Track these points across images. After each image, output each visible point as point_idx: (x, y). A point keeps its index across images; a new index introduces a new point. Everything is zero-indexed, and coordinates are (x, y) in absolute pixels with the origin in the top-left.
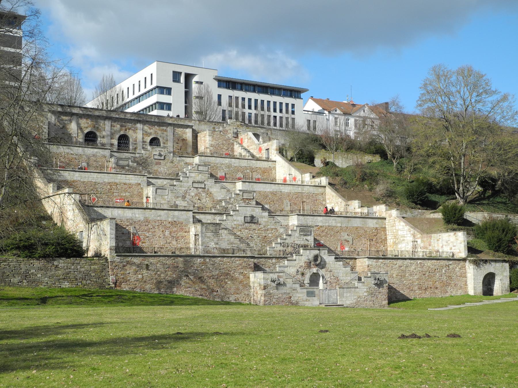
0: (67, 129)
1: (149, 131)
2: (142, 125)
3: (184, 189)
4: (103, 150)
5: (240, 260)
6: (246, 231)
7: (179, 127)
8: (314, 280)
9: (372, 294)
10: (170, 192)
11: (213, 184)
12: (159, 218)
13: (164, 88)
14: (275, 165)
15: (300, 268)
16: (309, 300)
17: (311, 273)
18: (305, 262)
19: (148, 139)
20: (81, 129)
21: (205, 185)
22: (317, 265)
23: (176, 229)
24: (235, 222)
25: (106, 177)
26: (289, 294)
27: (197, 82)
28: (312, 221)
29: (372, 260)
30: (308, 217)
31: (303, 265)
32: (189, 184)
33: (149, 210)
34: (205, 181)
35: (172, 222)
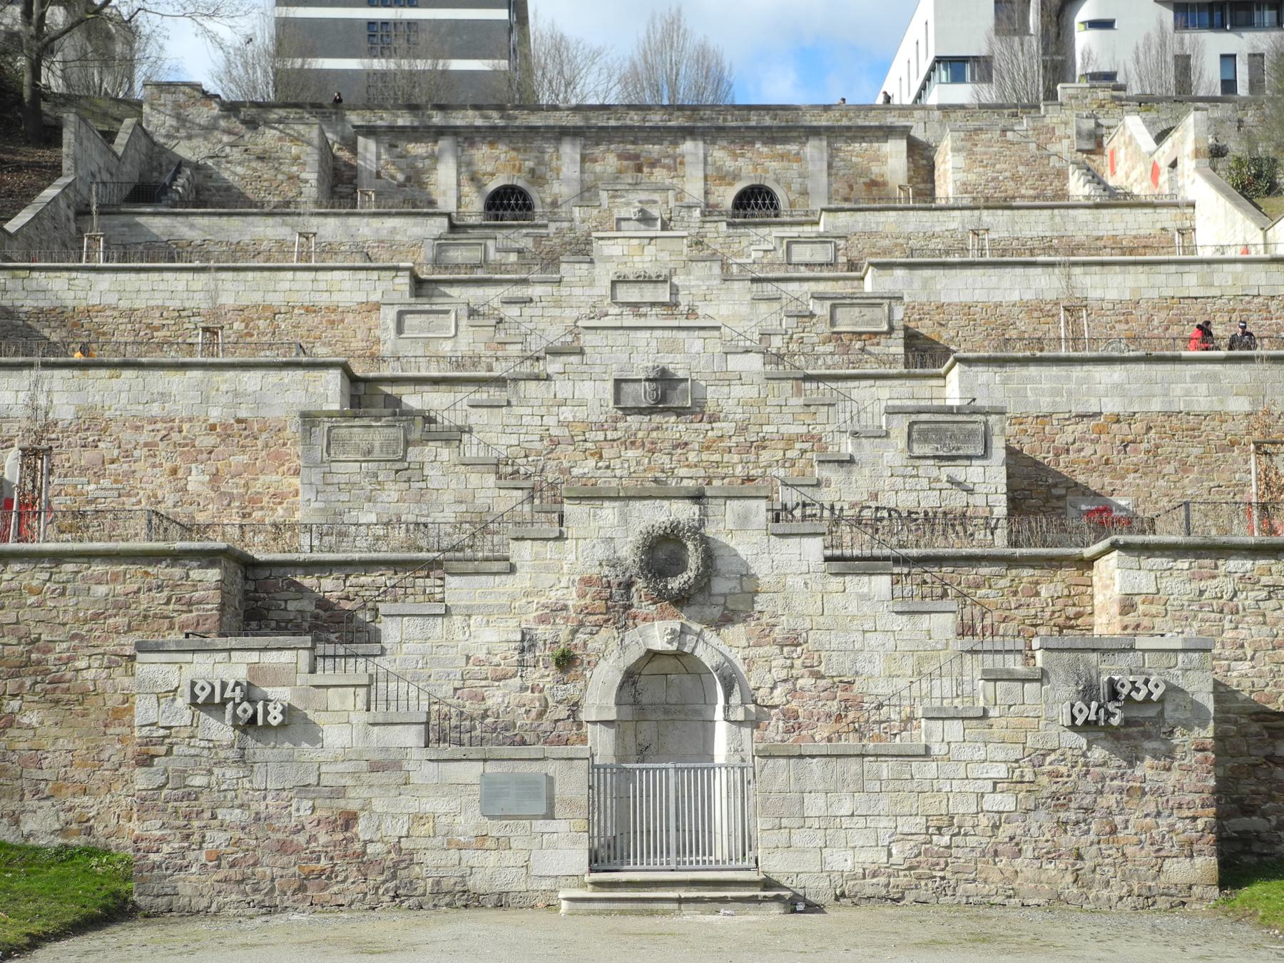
0: (422, 185)
1: (729, 164)
2: (701, 144)
3: (570, 314)
4: (420, 220)
5: (115, 578)
6: (630, 453)
7: (853, 139)
8: (663, 703)
9: (1060, 801)
10: (464, 322)
11: (716, 282)
12: (155, 409)
13: (963, 60)
14: (1192, 219)
15: (542, 620)
16: (503, 844)
17: (634, 655)
18: (588, 582)
19: (727, 195)
20: (474, 179)
21: (674, 290)
22: (681, 600)
23: (244, 458)
24: (567, 413)
25: (228, 285)
26: (339, 792)
27: (1094, 24)
28: (1055, 393)
29: (1160, 562)
30: (1033, 370)
31: (573, 600)
32: (596, 291)
33: (104, 373)
34: (673, 272)
35: (226, 427)
